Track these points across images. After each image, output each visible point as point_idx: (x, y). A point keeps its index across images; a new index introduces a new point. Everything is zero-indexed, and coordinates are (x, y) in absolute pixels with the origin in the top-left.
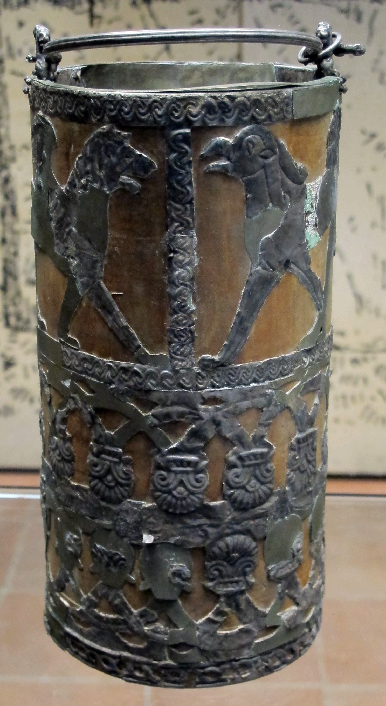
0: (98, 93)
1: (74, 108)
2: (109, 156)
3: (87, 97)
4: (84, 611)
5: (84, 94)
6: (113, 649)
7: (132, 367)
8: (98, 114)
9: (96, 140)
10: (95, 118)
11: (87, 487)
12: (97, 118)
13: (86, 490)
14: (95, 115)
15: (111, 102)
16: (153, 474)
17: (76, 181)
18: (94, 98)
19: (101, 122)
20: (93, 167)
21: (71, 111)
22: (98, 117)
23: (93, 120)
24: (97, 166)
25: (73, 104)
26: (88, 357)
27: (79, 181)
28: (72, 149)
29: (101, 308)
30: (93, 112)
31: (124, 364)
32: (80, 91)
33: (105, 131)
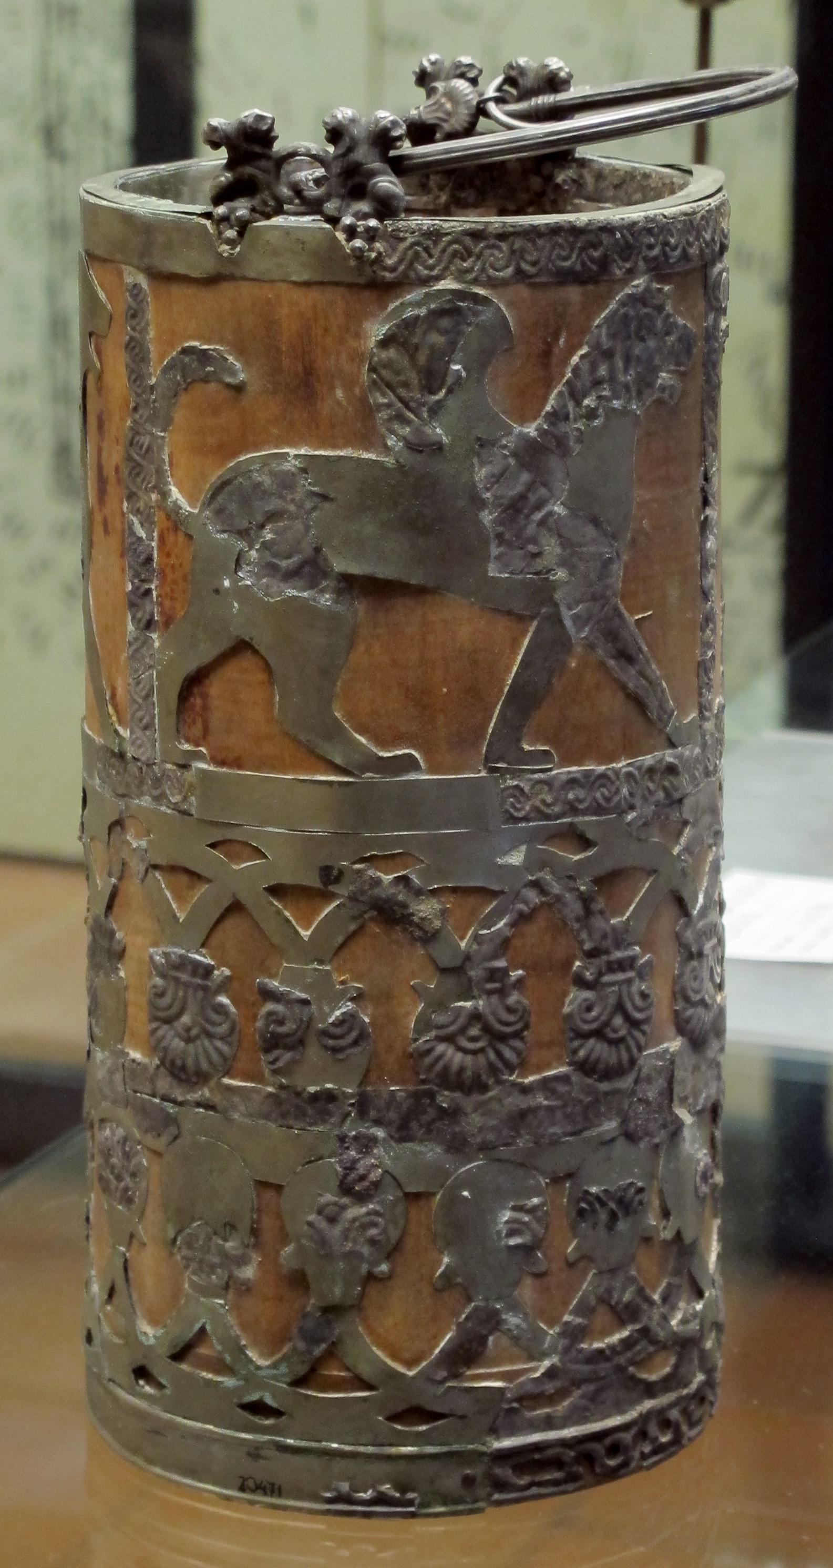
0: (628, 218)
1: (574, 256)
2: (642, 339)
3: (607, 229)
4: (559, 1364)
5: (600, 224)
6: (622, 1412)
7: (661, 761)
8: (626, 260)
9: (622, 311)
10: (620, 269)
11: (563, 1069)
12: (624, 267)
13: (564, 1079)
14: (620, 263)
15: (649, 231)
16: (681, 975)
17: (571, 406)
18: (621, 228)
19: (631, 273)
20: (612, 371)
21: (567, 264)
22: (628, 266)
23: (618, 272)
24: (620, 364)
25: (572, 250)
26: (578, 775)
27: (578, 404)
28: (562, 341)
29: (614, 657)
30: (616, 258)
31: (648, 760)
32: (590, 221)
33: (641, 289)
